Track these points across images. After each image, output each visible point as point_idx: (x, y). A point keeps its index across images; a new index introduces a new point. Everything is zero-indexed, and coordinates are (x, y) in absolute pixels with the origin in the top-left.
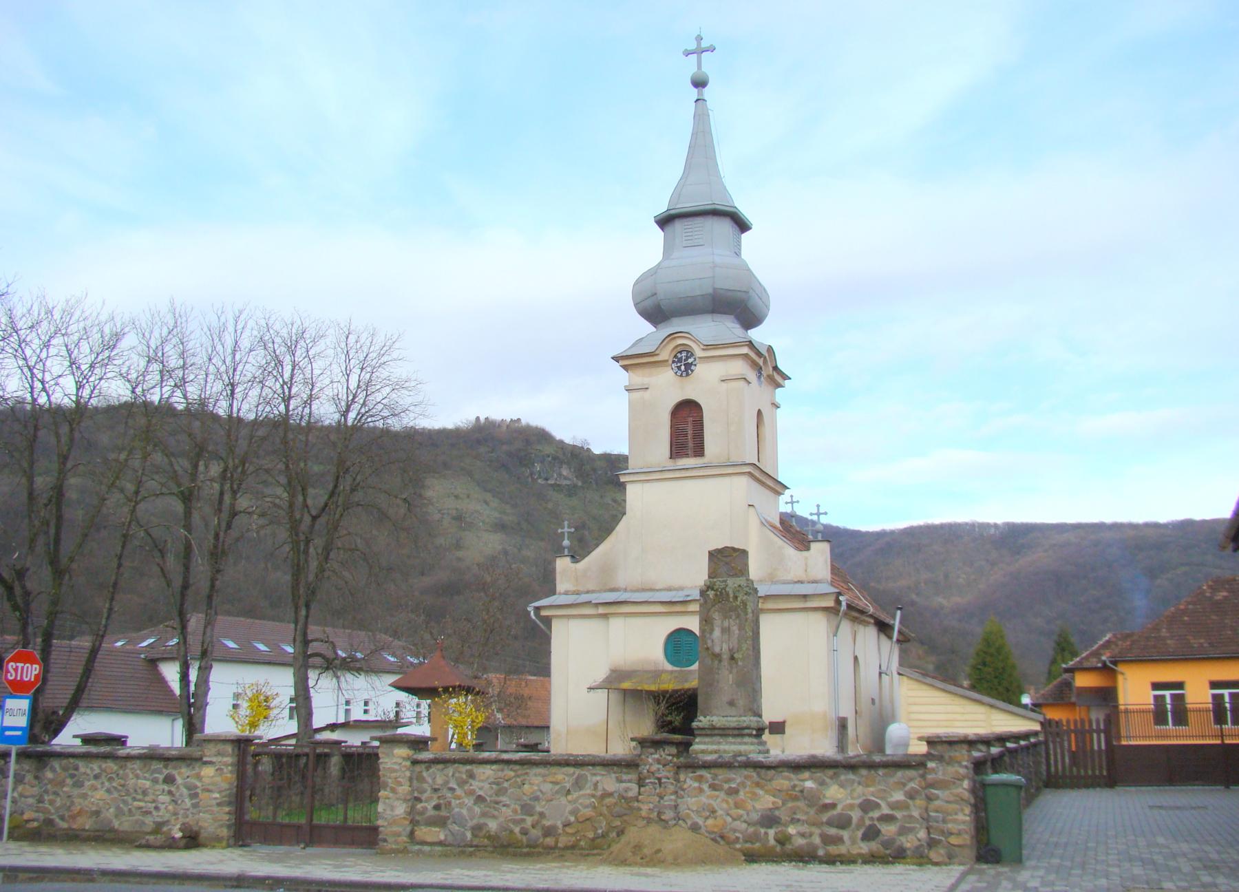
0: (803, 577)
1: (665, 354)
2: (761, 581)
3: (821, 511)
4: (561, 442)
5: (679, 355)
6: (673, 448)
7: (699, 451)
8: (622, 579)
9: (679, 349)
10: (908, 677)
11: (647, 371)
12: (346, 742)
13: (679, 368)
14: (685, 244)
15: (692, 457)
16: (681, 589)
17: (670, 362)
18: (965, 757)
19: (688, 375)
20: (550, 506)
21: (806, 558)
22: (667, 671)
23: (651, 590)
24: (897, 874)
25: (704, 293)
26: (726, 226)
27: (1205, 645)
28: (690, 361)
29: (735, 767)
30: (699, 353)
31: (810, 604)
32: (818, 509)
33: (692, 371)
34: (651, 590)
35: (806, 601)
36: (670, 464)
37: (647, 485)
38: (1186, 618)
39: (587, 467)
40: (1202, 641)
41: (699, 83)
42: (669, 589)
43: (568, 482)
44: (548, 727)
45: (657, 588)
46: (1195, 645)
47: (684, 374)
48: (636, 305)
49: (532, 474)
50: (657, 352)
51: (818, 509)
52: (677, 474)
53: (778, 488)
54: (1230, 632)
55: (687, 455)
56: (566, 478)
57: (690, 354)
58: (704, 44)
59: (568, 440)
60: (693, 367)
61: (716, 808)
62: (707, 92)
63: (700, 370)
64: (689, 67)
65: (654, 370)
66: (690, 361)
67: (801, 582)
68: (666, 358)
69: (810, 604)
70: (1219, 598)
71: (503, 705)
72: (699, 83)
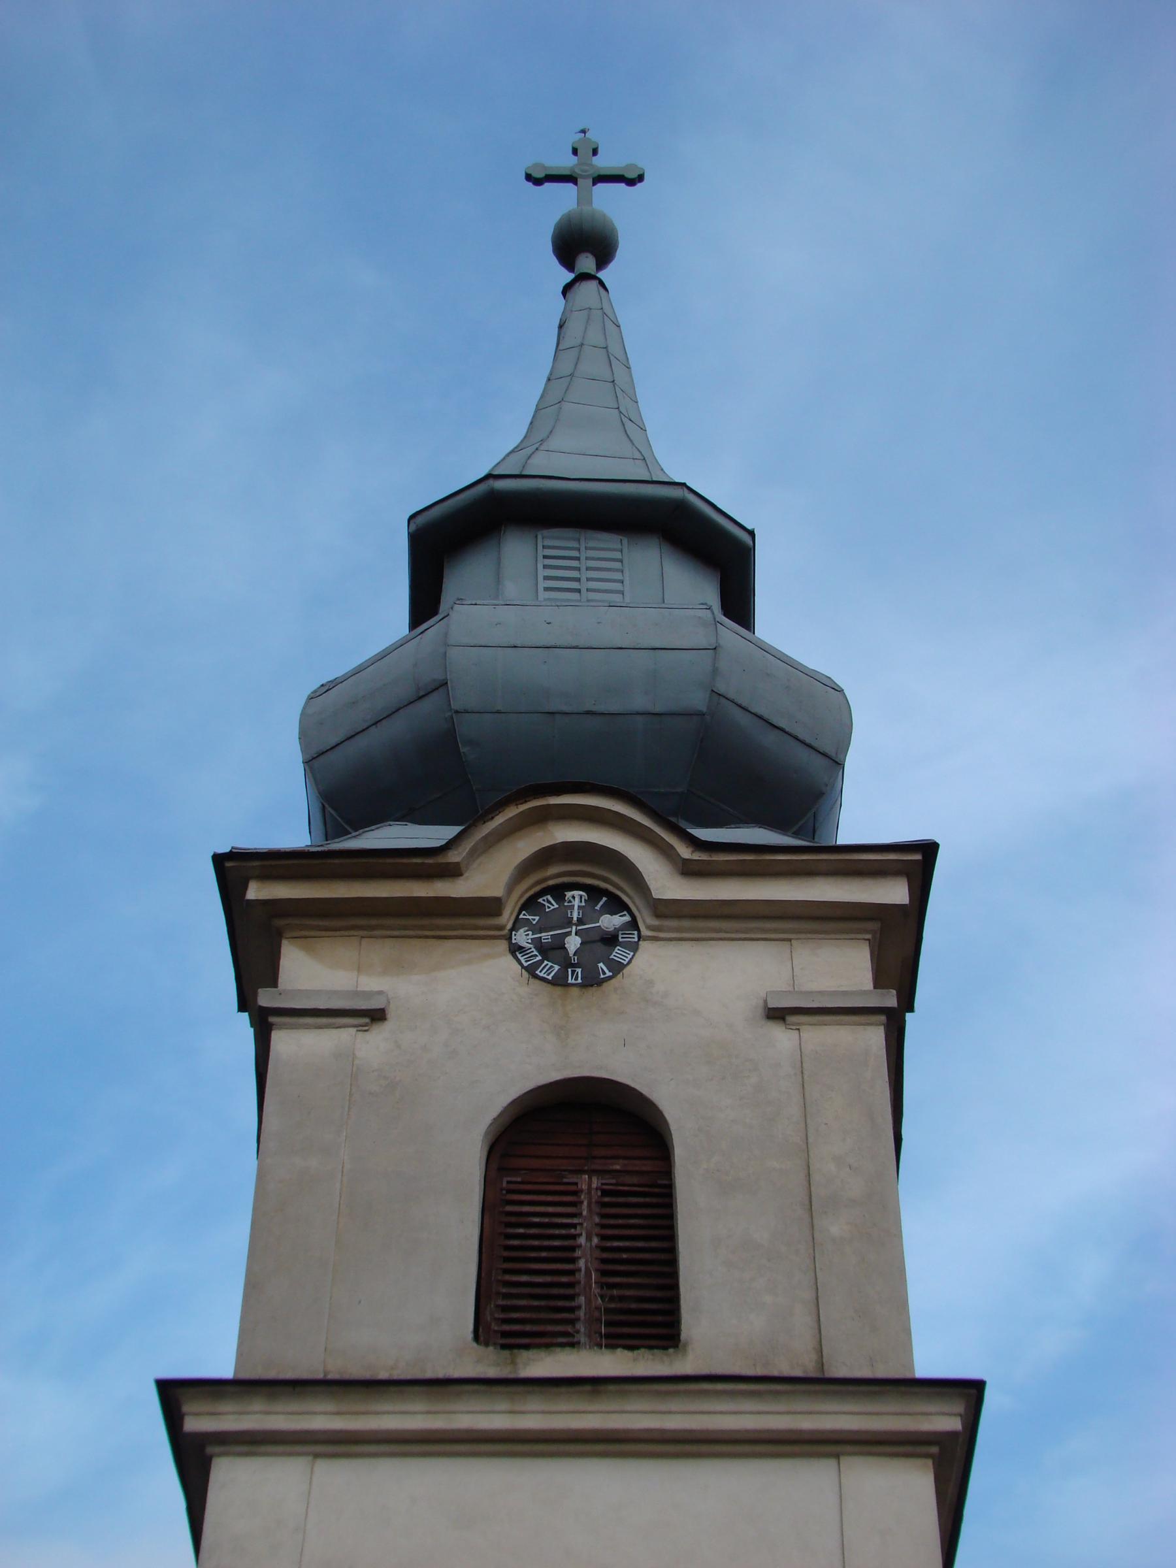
9: (554, 873)
11: (379, 951)
13: (552, 950)
19: (592, 981)
33: (617, 968)
47: (575, 977)
50: (454, 857)
58: (605, 162)
60: (618, 953)
68: (498, 891)
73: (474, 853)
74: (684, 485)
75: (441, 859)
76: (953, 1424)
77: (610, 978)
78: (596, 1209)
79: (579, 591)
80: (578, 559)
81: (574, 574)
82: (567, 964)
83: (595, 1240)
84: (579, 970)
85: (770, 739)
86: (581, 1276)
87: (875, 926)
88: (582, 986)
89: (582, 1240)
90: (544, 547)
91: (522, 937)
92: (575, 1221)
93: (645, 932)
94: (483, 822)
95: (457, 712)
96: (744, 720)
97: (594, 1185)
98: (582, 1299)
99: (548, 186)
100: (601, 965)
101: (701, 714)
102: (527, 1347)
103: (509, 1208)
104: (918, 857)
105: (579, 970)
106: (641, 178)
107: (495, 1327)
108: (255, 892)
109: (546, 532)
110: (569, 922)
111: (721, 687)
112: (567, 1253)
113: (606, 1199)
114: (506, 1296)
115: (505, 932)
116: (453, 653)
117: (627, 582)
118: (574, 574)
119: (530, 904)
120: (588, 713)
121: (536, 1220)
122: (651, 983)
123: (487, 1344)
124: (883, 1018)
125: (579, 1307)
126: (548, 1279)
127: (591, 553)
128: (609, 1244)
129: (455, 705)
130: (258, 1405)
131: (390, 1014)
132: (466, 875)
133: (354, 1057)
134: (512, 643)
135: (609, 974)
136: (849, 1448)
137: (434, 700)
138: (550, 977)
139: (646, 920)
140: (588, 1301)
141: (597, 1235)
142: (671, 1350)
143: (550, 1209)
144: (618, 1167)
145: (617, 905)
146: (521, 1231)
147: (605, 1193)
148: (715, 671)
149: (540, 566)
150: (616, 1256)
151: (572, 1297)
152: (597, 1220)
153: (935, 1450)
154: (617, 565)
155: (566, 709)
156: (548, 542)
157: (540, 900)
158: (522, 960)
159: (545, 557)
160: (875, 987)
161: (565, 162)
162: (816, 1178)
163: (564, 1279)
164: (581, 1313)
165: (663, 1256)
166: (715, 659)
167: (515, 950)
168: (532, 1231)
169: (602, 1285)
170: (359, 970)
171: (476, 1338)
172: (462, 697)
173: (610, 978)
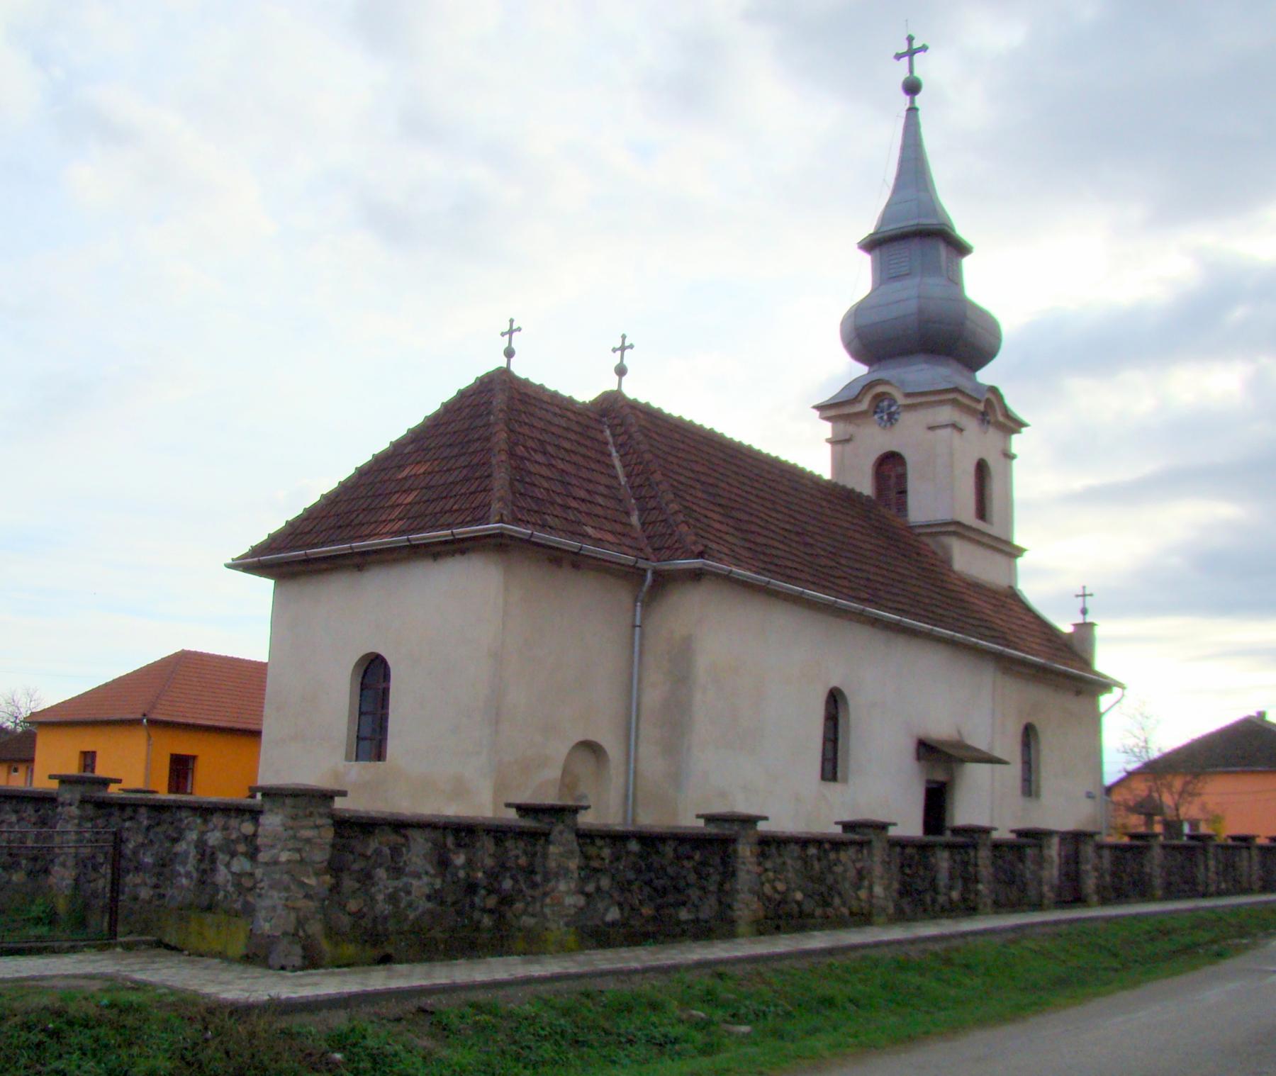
12: (119, 781)
13: (881, 418)
18: (275, 959)
24: (584, 479)
26: (942, 249)
29: (146, 806)
30: (901, 400)
33: (896, 420)
41: (912, 88)
44: (256, 734)
53: (1011, 424)
57: (893, 401)
58: (916, 45)
60: (896, 416)
62: (919, 100)
64: (900, 72)
66: (893, 409)
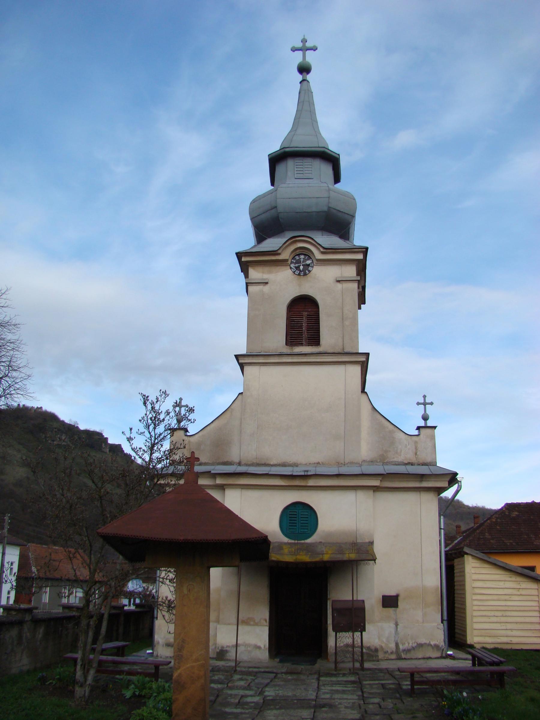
0: (414, 460)
1: (286, 255)
2: (372, 461)
3: (427, 401)
4: (63, 422)
5: (297, 258)
6: (288, 338)
7: (315, 340)
8: (234, 454)
9: (298, 252)
10: (472, 555)
11: (266, 269)
13: (298, 268)
14: (296, 176)
15: (305, 345)
16: (296, 465)
17: (289, 262)
19: (305, 274)
20: (63, 448)
21: (416, 442)
22: (286, 544)
23: (266, 465)
25: (318, 210)
26: (327, 170)
27: (514, 544)
28: (308, 262)
31: (425, 484)
32: (425, 400)
33: (310, 271)
34: (266, 465)
35: (421, 481)
36: (286, 350)
37: (264, 369)
38: (498, 527)
39: (76, 437)
40: (511, 541)
41: (304, 69)
42: (284, 465)
43: (65, 443)
45: (272, 463)
46: (508, 544)
47: (302, 274)
48: (252, 219)
49: (46, 437)
50: (279, 252)
51: (425, 400)
52: (295, 359)
54: (526, 537)
55: (302, 344)
56: (64, 441)
58: (308, 45)
59: (67, 421)
60: (310, 268)
61: (48, 611)
62: (309, 77)
63: (317, 271)
64: (298, 58)
65: (274, 269)
67: (412, 464)
68: (287, 258)
69: (425, 484)
70: (514, 515)
71: (165, 580)
72: (304, 69)
73: (283, 250)
74: (324, 147)
75: (277, 252)
76: (364, 359)
77: (308, 274)
78: (306, 318)
79: (303, 174)
80: (303, 165)
81: (302, 169)
82: (300, 271)
83: (306, 324)
84: (303, 272)
85: (340, 214)
86: (304, 331)
87: (357, 262)
88: (303, 275)
89: (304, 324)
90: (296, 163)
91: (292, 266)
92: (303, 321)
93: (315, 264)
94: (296, 464)
95: (279, 213)
96: (334, 211)
97: (306, 314)
98: (304, 335)
99: (296, 52)
100: (307, 271)
101: (326, 212)
102: (295, 346)
103: (291, 319)
104: (364, 250)
105: (303, 272)
106: (317, 49)
107: (289, 341)
108: (243, 259)
109: (296, 159)
110: (301, 263)
111: (330, 206)
112: (301, 327)
113: (308, 316)
114: (291, 335)
115: (289, 265)
116: (278, 200)
117: (313, 171)
118: (302, 169)
119: (293, 258)
120: (305, 212)
121: (296, 321)
122: (316, 275)
123: (288, 346)
124: (357, 282)
125: (303, 337)
126: (298, 332)
127: (306, 164)
128: (309, 325)
129: (278, 211)
130: (251, 358)
131: (269, 283)
132: (282, 254)
133: (263, 291)
134: (289, 198)
135: (308, 273)
136: (347, 363)
137: (273, 211)
138: (297, 274)
139: (315, 261)
140: (305, 336)
141: (307, 323)
142: (318, 346)
143: (298, 319)
144: (310, 310)
145: (310, 258)
146: (293, 323)
147: (308, 315)
148: (329, 202)
149: (295, 168)
150: (310, 327)
151: (302, 335)
152: (306, 320)
153: (361, 363)
154: (310, 166)
155: (300, 211)
156: (297, 161)
157: (295, 257)
158: (292, 270)
159: (296, 165)
160: (357, 276)
161: (300, 45)
162: (344, 313)
163: (301, 332)
164: (304, 338)
165: (317, 338)
166: (329, 200)
167: (291, 268)
168: (295, 323)
169: (307, 333)
170: (263, 273)
171: (286, 345)
172: (280, 209)
173: (308, 274)
